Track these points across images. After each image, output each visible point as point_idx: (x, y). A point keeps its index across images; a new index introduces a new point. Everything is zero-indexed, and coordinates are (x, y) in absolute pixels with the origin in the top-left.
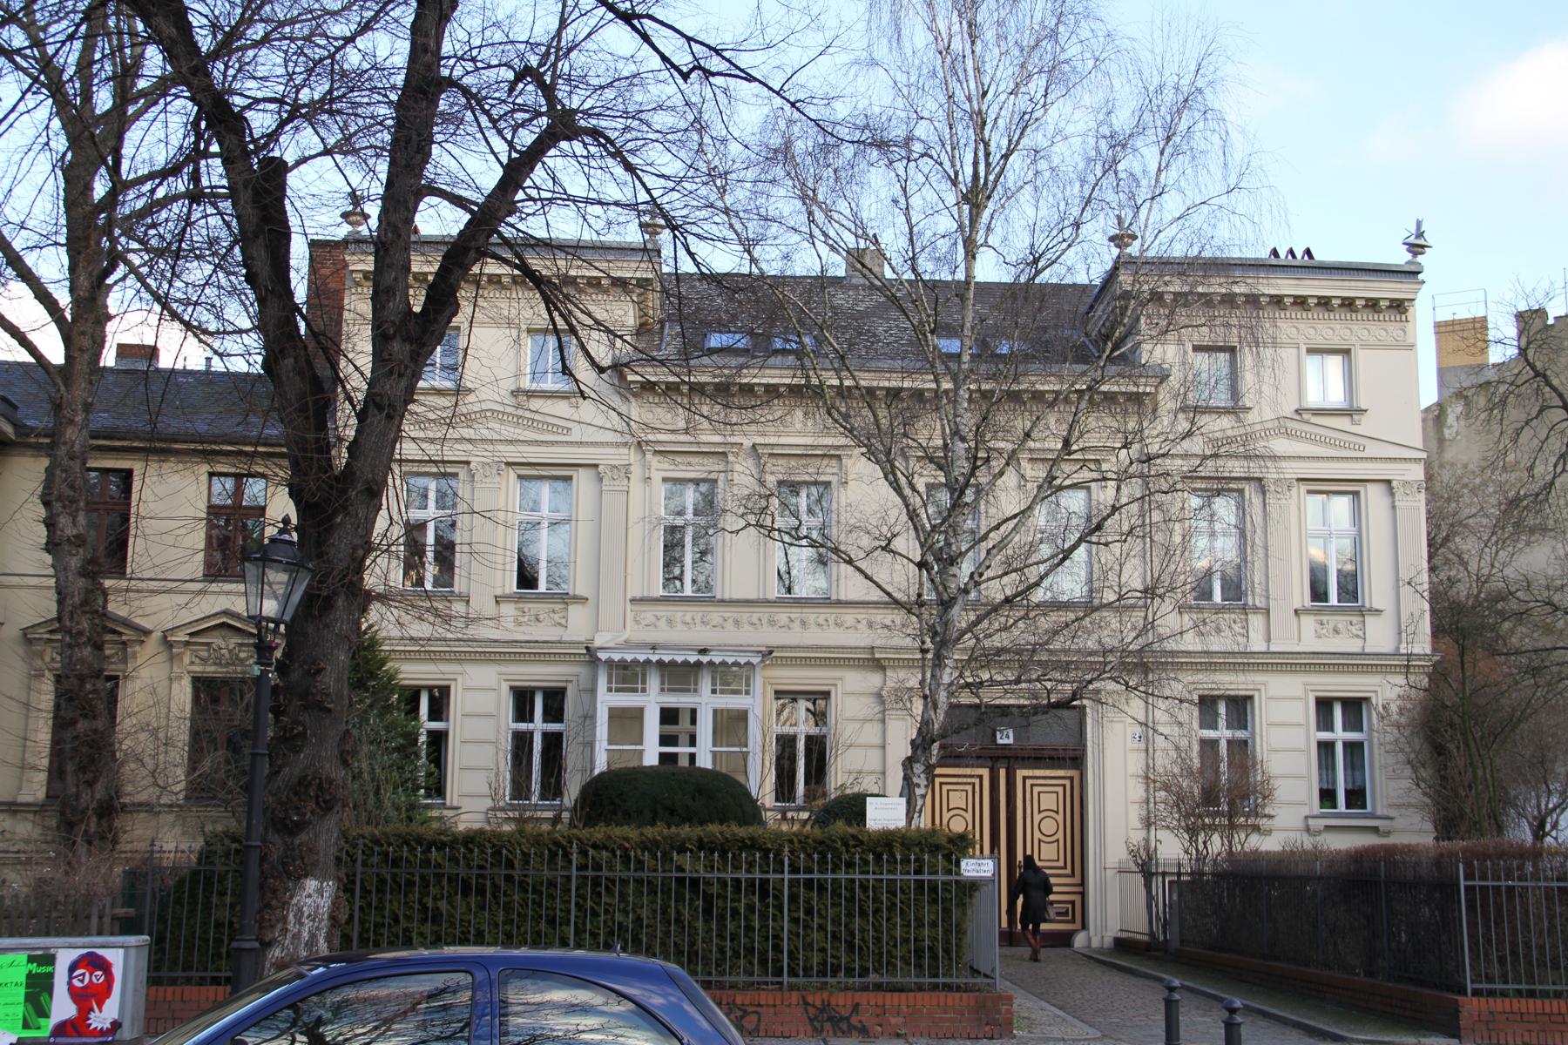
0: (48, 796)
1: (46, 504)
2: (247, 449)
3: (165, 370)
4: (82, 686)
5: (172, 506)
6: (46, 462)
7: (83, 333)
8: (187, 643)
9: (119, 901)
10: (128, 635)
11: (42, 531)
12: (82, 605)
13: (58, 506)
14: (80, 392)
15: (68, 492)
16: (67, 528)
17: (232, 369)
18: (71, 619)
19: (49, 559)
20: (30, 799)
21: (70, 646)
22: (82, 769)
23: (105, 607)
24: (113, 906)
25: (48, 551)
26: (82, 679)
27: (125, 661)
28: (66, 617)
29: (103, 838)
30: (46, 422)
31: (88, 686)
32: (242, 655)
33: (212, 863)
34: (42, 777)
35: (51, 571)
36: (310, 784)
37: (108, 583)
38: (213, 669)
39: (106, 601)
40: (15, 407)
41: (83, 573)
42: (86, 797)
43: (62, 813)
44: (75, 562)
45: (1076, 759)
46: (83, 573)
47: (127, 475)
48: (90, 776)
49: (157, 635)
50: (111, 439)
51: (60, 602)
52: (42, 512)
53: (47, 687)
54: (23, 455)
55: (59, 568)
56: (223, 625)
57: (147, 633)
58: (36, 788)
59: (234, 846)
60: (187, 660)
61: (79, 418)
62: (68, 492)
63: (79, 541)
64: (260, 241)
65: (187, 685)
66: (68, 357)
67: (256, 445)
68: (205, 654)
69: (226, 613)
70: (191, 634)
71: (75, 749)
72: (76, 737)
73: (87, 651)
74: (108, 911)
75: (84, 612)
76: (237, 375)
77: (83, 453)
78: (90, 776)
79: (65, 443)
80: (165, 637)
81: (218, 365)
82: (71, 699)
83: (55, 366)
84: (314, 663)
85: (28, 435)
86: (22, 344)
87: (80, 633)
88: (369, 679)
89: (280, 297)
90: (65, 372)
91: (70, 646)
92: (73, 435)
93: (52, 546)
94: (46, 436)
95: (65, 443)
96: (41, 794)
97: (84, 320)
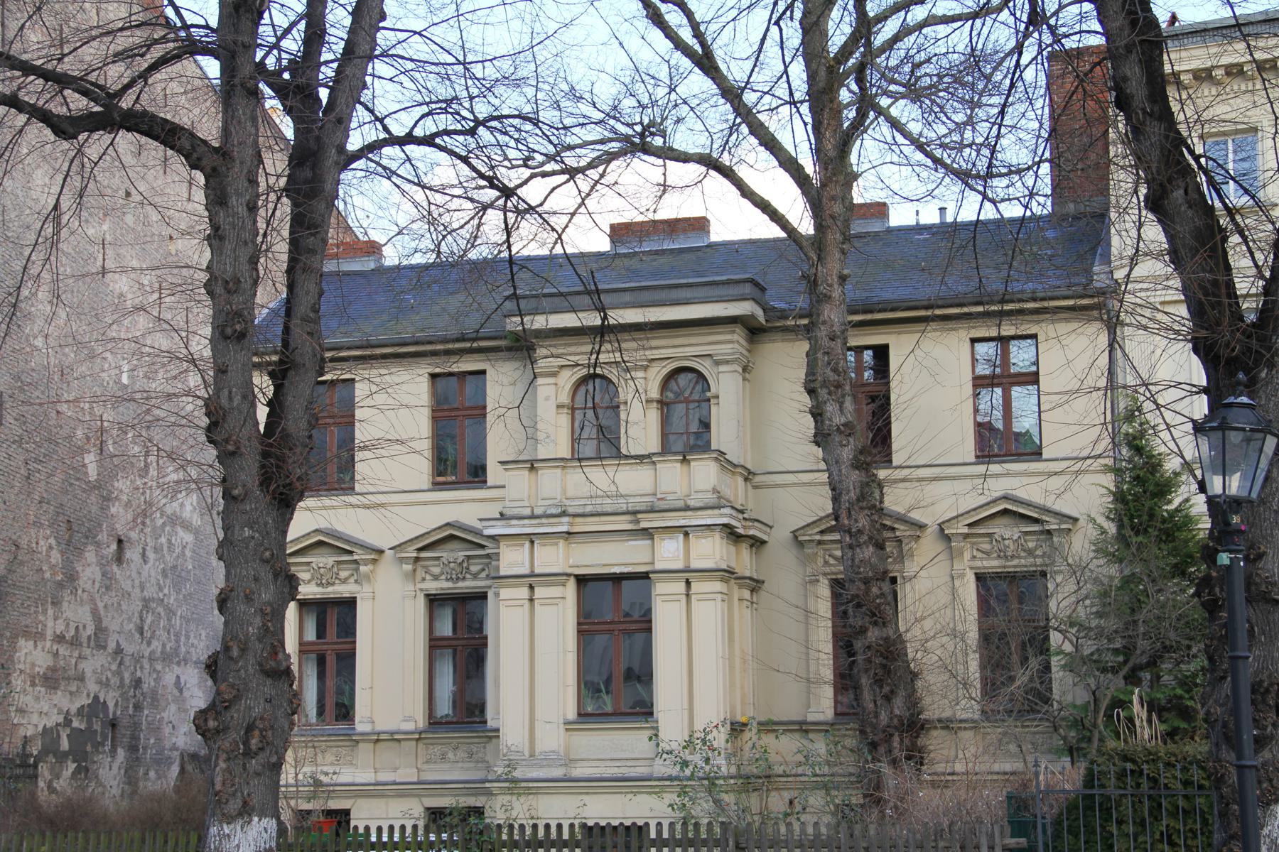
0: (836, 714)
1: (811, 392)
2: (994, 308)
3: (900, 229)
4: (868, 591)
5: (933, 380)
6: (806, 346)
7: (833, 198)
8: (966, 536)
9: (1008, 830)
10: (902, 531)
11: (809, 422)
12: (858, 500)
13: (823, 393)
14: (833, 266)
15: (832, 376)
16: (835, 416)
17: (1007, 215)
18: (849, 516)
19: (819, 452)
20: (821, 717)
21: (851, 547)
22: (879, 682)
23: (881, 502)
24: (1002, 835)
25: (818, 444)
26: (866, 581)
27: (901, 559)
28: (843, 516)
29: (909, 758)
30: (802, 302)
31: (875, 590)
32: (1031, 545)
33: (1102, 786)
34: (829, 692)
35: (823, 466)
36: (1267, 691)
37: (882, 474)
38: (996, 563)
39: (882, 494)
40: (763, 289)
41: (858, 465)
42: (884, 717)
43: (862, 732)
44: (846, 454)
45: (300, 644)
46: (858, 465)
47: (881, 353)
48: (886, 689)
49: (932, 529)
50: (872, 313)
51: (836, 500)
52: (806, 400)
53: (824, 590)
54: (774, 341)
55: (831, 462)
56: (1005, 512)
57: (922, 527)
58: (824, 705)
59: (1129, 766)
60: (967, 555)
61: (836, 294)
62: (832, 376)
63: (847, 430)
64: (1133, 56)
65: (971, 577)
66: (819, 226)
67: (1003, 301)
68: (986, 547)
69: (1005, 498)
70: (970, 525)
71: (869, 661)
72: (869, 647)
73: (868, 552)
74: (997, 840)
75: (862, 508)
76: (1012, 221)
77: (843, 332)
78: (886, 689)
79: (824, 323)
80: (942, 530)
81: (989, 213)
82: (859, 605)
83: (808, 238)
84: (1251, 547)
85: (786, 318)
86: (772, 219)
87: (860, 532)
88: (1189, 565)
89: (1160, 119)
90: (818, 241)
91: (851, 547)
92: (833, 315)
93: (820, 438)
94: (801, 317)
95: (824, 323)
96: (829, 714)
97: (829, 183)
